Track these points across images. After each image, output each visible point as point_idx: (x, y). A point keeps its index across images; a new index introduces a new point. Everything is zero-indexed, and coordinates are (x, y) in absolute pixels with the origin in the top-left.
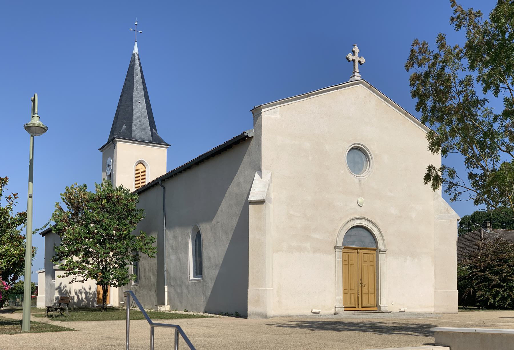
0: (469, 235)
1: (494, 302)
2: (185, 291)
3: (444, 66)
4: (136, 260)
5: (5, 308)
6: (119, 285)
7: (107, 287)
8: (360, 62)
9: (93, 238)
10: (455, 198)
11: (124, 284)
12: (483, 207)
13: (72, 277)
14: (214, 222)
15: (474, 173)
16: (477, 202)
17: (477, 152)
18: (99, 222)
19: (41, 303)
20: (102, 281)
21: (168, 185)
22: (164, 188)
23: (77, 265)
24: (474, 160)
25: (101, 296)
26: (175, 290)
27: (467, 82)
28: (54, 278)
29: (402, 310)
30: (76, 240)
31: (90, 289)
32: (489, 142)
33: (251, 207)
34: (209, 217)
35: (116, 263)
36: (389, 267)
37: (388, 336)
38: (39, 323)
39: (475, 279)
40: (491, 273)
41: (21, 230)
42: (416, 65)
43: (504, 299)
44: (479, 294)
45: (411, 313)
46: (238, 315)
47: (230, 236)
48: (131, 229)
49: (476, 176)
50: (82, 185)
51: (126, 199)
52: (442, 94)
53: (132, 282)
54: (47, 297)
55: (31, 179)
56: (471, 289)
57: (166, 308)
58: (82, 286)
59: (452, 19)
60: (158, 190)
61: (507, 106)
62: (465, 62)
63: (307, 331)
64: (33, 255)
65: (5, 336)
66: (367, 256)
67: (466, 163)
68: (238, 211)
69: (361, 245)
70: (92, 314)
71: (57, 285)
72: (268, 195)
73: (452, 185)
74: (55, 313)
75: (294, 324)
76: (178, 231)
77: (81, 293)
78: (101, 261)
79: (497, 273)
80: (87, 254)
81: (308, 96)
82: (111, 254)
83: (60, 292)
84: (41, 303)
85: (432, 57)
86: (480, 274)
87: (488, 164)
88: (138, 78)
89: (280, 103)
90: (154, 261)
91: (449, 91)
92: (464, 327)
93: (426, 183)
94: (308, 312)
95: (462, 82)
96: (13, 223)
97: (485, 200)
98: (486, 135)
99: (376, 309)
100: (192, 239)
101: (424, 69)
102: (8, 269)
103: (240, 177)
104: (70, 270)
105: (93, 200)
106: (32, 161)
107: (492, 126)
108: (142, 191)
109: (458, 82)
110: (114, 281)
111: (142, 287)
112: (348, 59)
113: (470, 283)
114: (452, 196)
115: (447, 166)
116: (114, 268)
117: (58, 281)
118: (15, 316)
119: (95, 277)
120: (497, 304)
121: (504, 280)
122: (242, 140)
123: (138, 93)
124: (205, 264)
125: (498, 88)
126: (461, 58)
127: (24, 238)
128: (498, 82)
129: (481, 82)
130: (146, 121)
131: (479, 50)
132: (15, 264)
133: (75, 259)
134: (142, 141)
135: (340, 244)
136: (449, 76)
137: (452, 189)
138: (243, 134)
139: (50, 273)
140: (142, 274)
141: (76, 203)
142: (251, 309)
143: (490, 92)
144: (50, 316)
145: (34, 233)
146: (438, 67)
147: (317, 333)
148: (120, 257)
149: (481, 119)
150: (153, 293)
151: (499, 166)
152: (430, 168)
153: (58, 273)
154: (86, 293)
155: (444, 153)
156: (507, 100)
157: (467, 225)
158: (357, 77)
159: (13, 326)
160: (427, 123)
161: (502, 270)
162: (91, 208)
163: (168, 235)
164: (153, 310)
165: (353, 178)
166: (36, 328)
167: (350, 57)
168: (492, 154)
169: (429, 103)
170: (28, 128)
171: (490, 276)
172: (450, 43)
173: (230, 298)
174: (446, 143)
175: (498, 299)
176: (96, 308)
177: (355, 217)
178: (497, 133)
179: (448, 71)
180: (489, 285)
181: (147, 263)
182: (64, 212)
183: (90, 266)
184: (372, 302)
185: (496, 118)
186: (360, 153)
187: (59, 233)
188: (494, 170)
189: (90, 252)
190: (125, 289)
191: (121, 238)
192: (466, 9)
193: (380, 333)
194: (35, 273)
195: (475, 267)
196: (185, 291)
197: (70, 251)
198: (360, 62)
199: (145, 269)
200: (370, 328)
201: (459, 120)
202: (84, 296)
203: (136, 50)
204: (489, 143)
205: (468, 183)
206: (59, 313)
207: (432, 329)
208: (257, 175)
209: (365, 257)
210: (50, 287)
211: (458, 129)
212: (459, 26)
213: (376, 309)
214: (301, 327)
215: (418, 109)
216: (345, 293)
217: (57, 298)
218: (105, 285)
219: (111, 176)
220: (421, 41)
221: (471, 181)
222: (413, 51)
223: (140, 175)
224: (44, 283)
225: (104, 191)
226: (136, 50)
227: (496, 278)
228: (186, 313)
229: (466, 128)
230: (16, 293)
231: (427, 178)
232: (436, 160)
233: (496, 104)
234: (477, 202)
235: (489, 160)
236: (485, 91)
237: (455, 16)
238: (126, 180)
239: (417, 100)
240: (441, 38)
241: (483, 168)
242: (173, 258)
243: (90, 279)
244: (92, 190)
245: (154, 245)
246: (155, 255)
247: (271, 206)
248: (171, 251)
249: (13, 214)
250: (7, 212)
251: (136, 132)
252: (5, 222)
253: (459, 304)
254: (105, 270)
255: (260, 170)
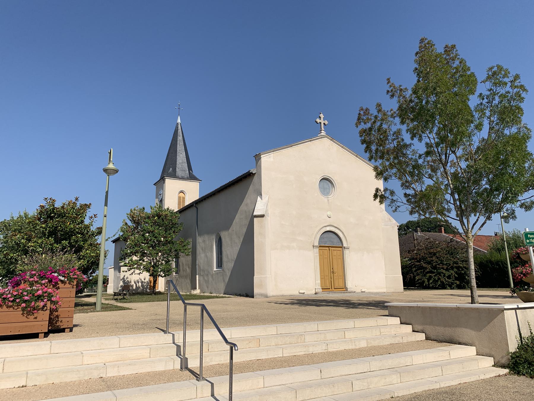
0: (405, 237)
1: (429, 284)
2: (210, 279)
3: (382, 123)
4: (177, 257)
5: (84, 294)
6: (165, 276)
7: (156, 278)
8: (324, 124)
9: (147, 243)
10: (396, 210)
11: (168, 275)
12: (415, 218)
13: (132, 271)
14: (230, 230)
15: (408, 193)
16: (411, 213)
17: (409, 179)
18: (152, 232)
19: (111, 290)
20: (153, 273)
21: (200, 206)
22: (197, 208)
23: (136, 263)
24: (407, 184)
25: (152, 284)
26: (204, 278)
27: (398, 133)
28: (120, 272)
29: (363, 290)
30: (136, 245)
31: (145, 279)
32: (416, 172)
33: (255, 219)
34: (227, 227)
35: (163, 260)
36: (352, 259)
37: (354, 310)
38: (108, 304)
39: (414, 267)
40: (424, 263)
41: (100, 239)
42: (362, 123)
43: (435, 281)
44: (417, 278)
45: (370, 293)
46: (247, 296)
47: (242, 240)
48: (174, 236)
49: (409, 195)
50: (141, 207)
51: (171, 216)
52: (381, 142)
53: (174, 274)
54: (114, 286)
55: (106, 205)
56: (412, 275)
57: (197, 292)
58: (139, 277)
59: (388, 91)
60: (193, 209)
61: (427, 148)
62: (398, 120)
63: (296, 306)
64: (105, 256)
65: (83, 314)
66: (336, 252)
67: (402, 186)
68: (247, 222)
69: (331, 243)
70: (146, 297)
71: (122, 277)
72: (267, 211)
73: (393, 201)
74: (120, 297)
75: (288, 301)
76: (206, 237)
77: (138, 282)
78: (153, 259)
79: (429, 263)
80: (143, 255)
81: (291, 146)
82: (160, 254)
83: (124, 282)
84: (111, 290)
85: (373, 118)
86: (417, 264)
87: (418, 187)
88: (180, 138)
89: (273, 151)
90: (190, 258)
91: (387, 139)
92: (409, 302)
93: (375, 200)
94: (296, 293)
95: (395, 133)
96: (93, 235)
97: (417, 211)
98: (414, 167)
99: (344, 290)
100: (216, 242)
101: (369, 125)
102: (88, 266)
103: (247, 200)
104: (131, 266)
105: (149, 218)
106: (107, 192)
107: (418, 161)
108: (181, 211)
109: (392, 133)
110: (162, 273)
111: (180, 277)
112: (316, 122)
113: (410, 270)
114: (394, 208)
115: (389, 188)
116: (162, 264)
117: (122, 275)
118: (91, 300)
119: (148, 271)
120: (431, 285)
121: (435, 268)
122: (248, 176)
123: (180, 147)
124: (225, 259)
125: (421, 136)
126: (395, 117)
127: (100, 244)
128: (420, 132)
129: (409, 133)
130: (186, 165)
131: (406, 112)
132: (93, 263)
133: (135, 258)
134: (183, 178)
135: (317, 244)
136: (386, 129)
137: (394, 204)
138: (249, 171)
139: (117, 268)
140: (181, 268)
141: (137, 220)
142: (256, 291)
143: (416, 139)
144: (116, 299)
145: (107, 240)
146: (378, 124)
147: (303, 308)
148: (166, 256)
149: (410, 157)
150: (188, 281)
151: (425, 188)
152: (377, 190)
153: (123, 269)
154: (142, 282)
155: (386, 179)
156: (427, 144)
157: (404, 230)
158: (323, 133)
159: (89, 307)
160: (373, 160)
161: (432, 261)
162: (147, 223)
163: (199, 240)
164: (188, 293)
165: (323, 199)
166: (106, 308)
167: (318, 120)
168: (420, 179)
169: (374, 148)
170: (105, 170)
171: (424, 265)
172: (384, 108)
173: (242, 284)
174: (387, 173)
175: (431, 281)
176: (149, 292)
177: (326, 225)
178: (421, 166)
179: (385, 126)
180: (424, 271)
181: (185, 260)
182: (129, 227)
183: (145, 263)
184: (341, 285)
185: (420, 156)
186: (327, 182)
187: (124, 240)
188: (421, 191)
189: (146, 253)
190: (168, 278)
191: (167, 243)
192: (397, 85)
193: (348, 307)
194: (106, 269)
195: (413, 259)
196: (210, 279)
197: (131, 252)
198: (324, 124)
199: (183, 264)
200: (343, 304)
201: (395, 158)
202: (140, 284)
203: (179, 121)
204: (417, 172)
205: (404, 200)
206: (122, 297)
207: (386, 304)
208: (259, 198)
209: (335, 253)
210: (117, 278)
211: (395, 164)
212: (392, 96)
213: (344, 290)
214: (293, 304)
215: (366, 152)
216: (322, 278)
217: (121, 286)
218: (155, 276)
219: (161, 201)
220: (364, 108)
221: (406, 199)
222: (359, 114)
223: (181, 200)
224: (113, 275)
225: (156, 211)
226: (179, 121)
227: (429, 266)
228: (211, 295)
229: (400, 163)
230: (94, 284)
231: (376, 196)
232: (380, 184)
233: (420, 147)
234: (411, 213)
235: (417, 184)
236: (412, 139)
237: (390, 90)
238: (172, 204)
239: (365, 145)
240: (379, 105)
241: (415, 190)
242: (203, 255)
243: (145, 273)
244: (148, 211)
245: (190, 246)
246: (190, 254)
247: (269, 218)
248: (201, 251)
249: (93, 228)
250: (89, 227)
251: (179, 173)
252: (87, 234)
253: (404, 286)
254: (155, 266)
255: (261, 195)
